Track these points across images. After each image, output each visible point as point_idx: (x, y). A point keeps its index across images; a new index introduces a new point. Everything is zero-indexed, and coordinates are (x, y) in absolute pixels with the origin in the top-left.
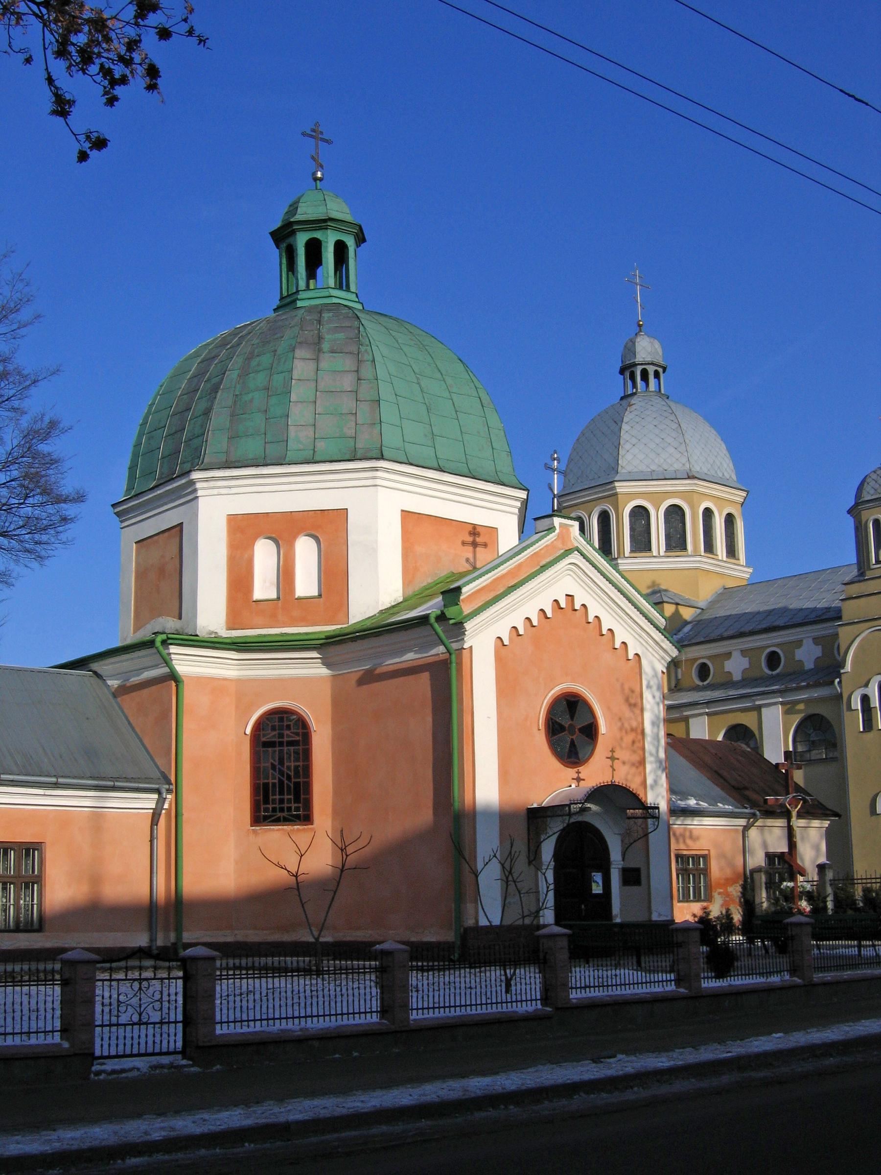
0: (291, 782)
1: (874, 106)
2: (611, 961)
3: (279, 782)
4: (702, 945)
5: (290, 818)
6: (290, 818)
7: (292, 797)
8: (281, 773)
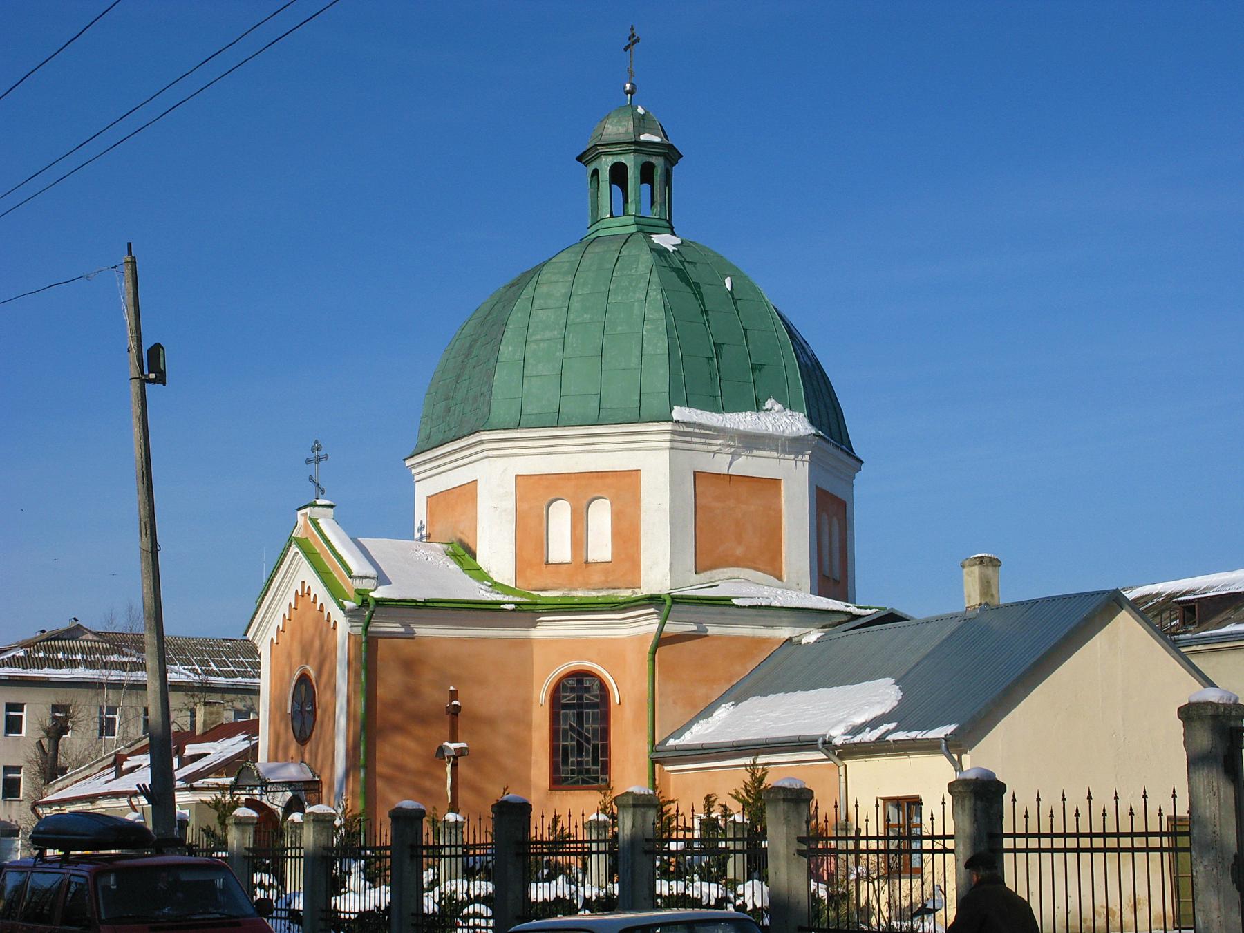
0: (589, 744)
1: (98, 15)
2: (474, 881)
3: (590, 742)
4: (766, 848)
5: (591, 781)
6: (591, 781)
7: (590, 759)
8: (580, 734)
